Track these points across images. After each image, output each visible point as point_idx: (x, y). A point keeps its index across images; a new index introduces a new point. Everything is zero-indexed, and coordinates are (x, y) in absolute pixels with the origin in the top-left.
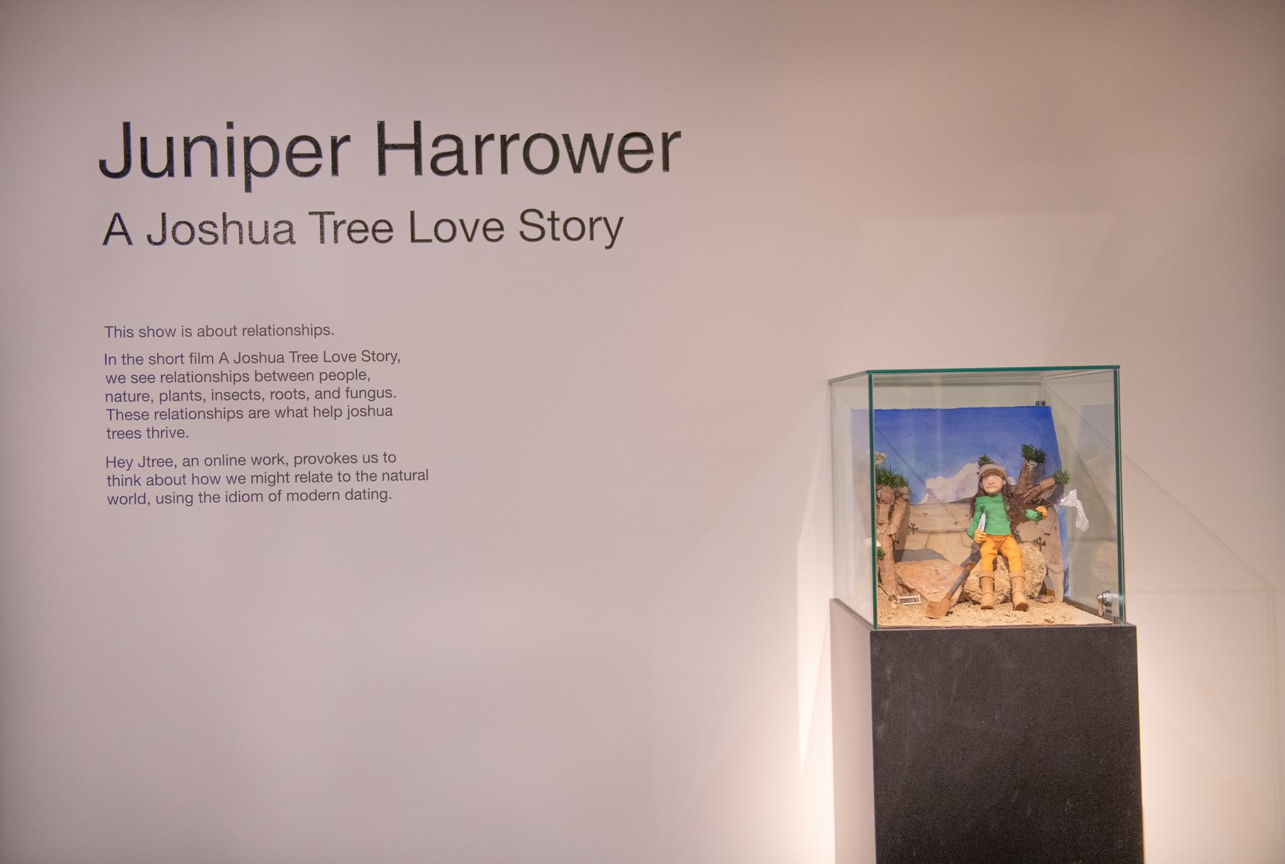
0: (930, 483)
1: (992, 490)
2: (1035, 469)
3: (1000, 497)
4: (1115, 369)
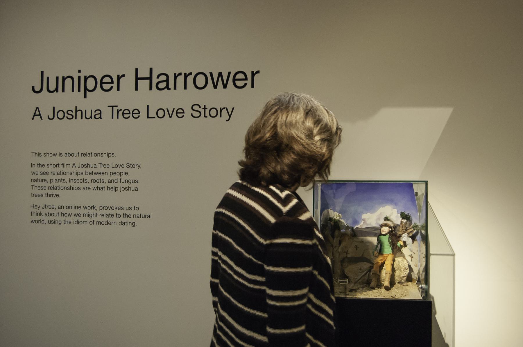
0: (364, 216)
1: (383, 233)
2: (406, 223)
3: (387, 236)
4: (426, 182)
